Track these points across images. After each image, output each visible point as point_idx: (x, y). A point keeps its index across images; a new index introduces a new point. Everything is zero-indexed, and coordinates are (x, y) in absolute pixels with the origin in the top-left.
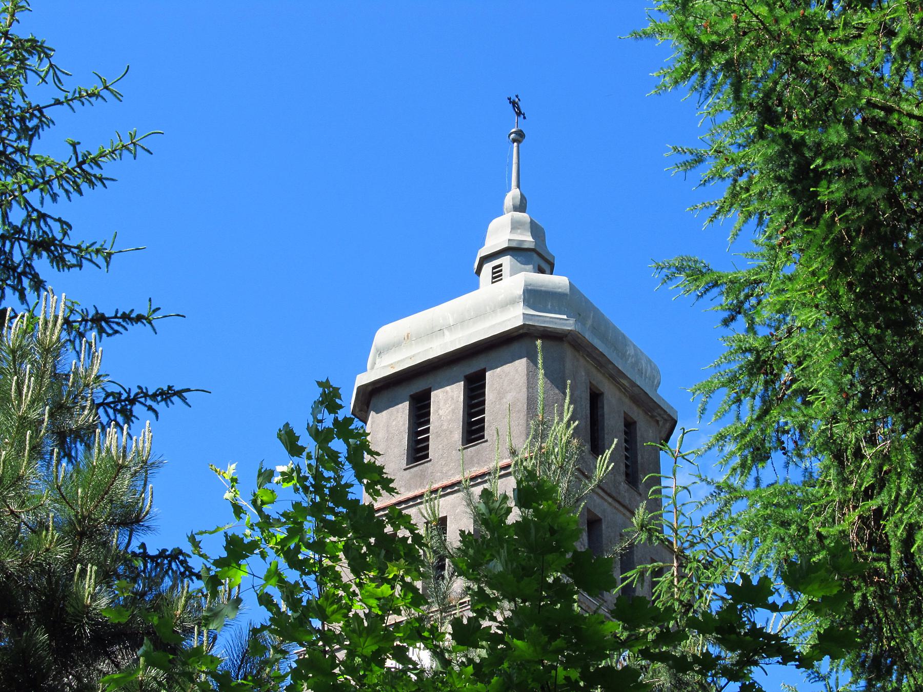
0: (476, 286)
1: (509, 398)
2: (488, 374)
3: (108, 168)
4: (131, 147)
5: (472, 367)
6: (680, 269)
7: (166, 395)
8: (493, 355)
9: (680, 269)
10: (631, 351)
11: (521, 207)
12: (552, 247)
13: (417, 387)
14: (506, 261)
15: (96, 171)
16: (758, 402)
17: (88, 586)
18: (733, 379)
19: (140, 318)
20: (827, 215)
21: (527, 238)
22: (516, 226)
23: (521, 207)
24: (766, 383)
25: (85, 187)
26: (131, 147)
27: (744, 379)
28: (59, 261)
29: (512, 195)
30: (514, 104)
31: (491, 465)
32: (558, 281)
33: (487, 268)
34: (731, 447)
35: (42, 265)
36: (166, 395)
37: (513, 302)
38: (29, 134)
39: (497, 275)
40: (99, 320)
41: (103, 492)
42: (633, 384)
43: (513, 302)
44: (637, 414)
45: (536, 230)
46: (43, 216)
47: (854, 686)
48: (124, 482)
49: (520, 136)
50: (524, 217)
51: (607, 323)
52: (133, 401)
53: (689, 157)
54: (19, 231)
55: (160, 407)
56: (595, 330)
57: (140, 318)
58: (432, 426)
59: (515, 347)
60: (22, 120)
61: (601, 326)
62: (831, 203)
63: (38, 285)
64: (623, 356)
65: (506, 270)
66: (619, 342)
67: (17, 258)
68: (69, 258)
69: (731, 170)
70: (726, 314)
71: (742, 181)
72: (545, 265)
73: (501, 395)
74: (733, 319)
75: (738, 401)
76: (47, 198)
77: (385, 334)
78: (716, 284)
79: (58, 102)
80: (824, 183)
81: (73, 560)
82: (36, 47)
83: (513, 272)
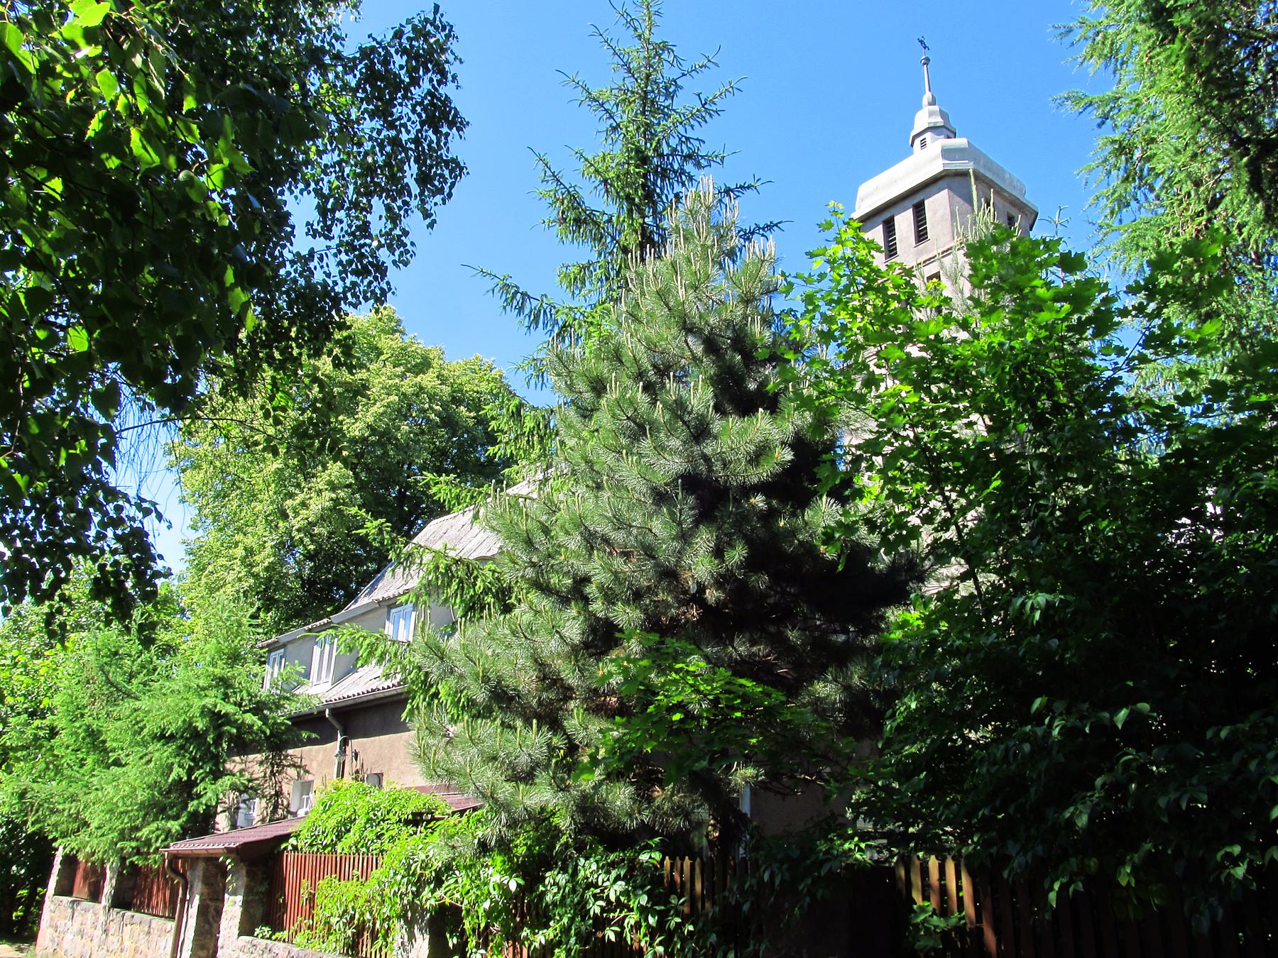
0: (911, 153)
1: (940, 213)
2: (926, 202)
3: (720, 104)
4: (732, 89)
5: (916, 200)
6: (1067, 99)
7: (770, 227)
8: (928, 190)
9: (1067, 99)
10: (1007, 176)
11: (933, 103)
12: (953, 124)
13: (886, 216)
14: (928, 135)
15: (714, 108)
16: (1121, 173)
17: (757, 328)
18: (1105, 160)
19: (749, 187)
20: (1180, 34)
21: (939, 121)
22: (931, 114)
23: (933, 103)
24: (1127, 160)
25: (707, 118)
26: (732, 89)
27: (1112, 161)
28: (698, 165)
29: (927, 96)
30: (921, 42)
31: (935, 253)
32: (960, 142)
33: (917, 142)
34: (1103, 202)
35: (689, 167)
36: (770, 227)
37: (935, 158)
38: (670, 96)
39: (923, 144)
40: (728, 191)
41: (755, 277)
42: (1011, 195)
43: (935, 158)
44: (1013, 211)
45: (943, 114)
46: (688, 139)
47: (574, 542)
48: (766, 270)
49: (927, 60)
50: (936, 108)
51: (992, 162)
52: (753, 233)
53: (1063, 30)
54: (675, 150)
55: (768, 233)
56: (984, 166)
57: (749, 187)
58: (897, 236)
59: (940, 183)
60: (666, 88)
61: (989, 164)
62: (1183, 27)
63: (691, 178)
64: (1003, 179)
65: (928, 141)
66: (1000, 171)
67: (676, 166)
68: (703, 162)
69: (1091, 34)
70: (1099, 121)
71: (1099, 38)
72: (952, 134)
73: (935, 213)
74: (1103, 123)
75: (1109, 173)
76: (689, 128)
77: (864, 189)
78: (1091, 104)
79: (684, 75)
80: (1176, 15)
81: (745, 317)
82: (665, 47)
83: (933, 141)
